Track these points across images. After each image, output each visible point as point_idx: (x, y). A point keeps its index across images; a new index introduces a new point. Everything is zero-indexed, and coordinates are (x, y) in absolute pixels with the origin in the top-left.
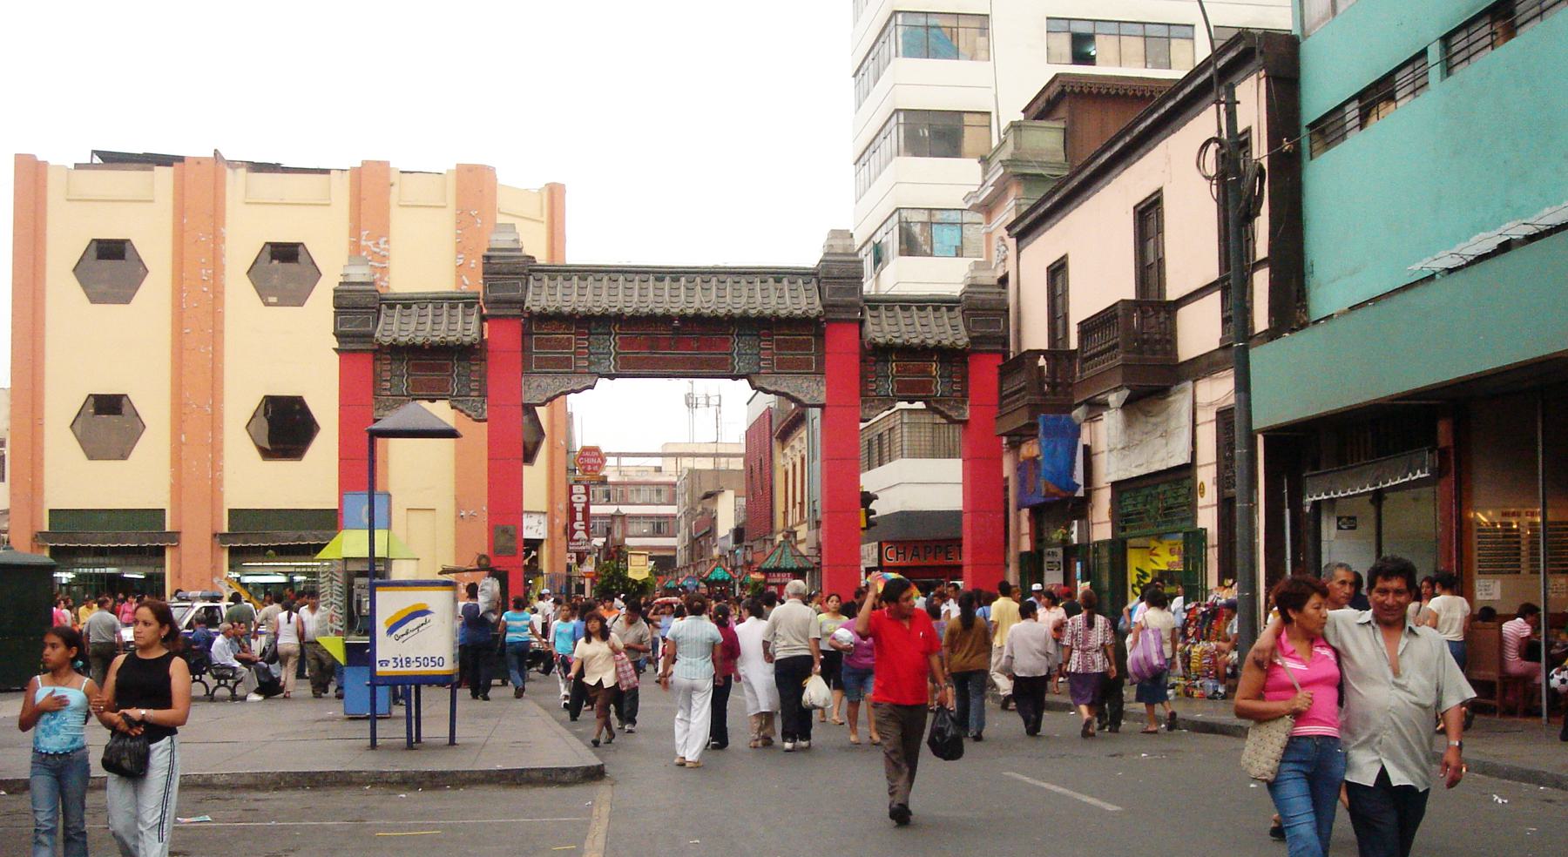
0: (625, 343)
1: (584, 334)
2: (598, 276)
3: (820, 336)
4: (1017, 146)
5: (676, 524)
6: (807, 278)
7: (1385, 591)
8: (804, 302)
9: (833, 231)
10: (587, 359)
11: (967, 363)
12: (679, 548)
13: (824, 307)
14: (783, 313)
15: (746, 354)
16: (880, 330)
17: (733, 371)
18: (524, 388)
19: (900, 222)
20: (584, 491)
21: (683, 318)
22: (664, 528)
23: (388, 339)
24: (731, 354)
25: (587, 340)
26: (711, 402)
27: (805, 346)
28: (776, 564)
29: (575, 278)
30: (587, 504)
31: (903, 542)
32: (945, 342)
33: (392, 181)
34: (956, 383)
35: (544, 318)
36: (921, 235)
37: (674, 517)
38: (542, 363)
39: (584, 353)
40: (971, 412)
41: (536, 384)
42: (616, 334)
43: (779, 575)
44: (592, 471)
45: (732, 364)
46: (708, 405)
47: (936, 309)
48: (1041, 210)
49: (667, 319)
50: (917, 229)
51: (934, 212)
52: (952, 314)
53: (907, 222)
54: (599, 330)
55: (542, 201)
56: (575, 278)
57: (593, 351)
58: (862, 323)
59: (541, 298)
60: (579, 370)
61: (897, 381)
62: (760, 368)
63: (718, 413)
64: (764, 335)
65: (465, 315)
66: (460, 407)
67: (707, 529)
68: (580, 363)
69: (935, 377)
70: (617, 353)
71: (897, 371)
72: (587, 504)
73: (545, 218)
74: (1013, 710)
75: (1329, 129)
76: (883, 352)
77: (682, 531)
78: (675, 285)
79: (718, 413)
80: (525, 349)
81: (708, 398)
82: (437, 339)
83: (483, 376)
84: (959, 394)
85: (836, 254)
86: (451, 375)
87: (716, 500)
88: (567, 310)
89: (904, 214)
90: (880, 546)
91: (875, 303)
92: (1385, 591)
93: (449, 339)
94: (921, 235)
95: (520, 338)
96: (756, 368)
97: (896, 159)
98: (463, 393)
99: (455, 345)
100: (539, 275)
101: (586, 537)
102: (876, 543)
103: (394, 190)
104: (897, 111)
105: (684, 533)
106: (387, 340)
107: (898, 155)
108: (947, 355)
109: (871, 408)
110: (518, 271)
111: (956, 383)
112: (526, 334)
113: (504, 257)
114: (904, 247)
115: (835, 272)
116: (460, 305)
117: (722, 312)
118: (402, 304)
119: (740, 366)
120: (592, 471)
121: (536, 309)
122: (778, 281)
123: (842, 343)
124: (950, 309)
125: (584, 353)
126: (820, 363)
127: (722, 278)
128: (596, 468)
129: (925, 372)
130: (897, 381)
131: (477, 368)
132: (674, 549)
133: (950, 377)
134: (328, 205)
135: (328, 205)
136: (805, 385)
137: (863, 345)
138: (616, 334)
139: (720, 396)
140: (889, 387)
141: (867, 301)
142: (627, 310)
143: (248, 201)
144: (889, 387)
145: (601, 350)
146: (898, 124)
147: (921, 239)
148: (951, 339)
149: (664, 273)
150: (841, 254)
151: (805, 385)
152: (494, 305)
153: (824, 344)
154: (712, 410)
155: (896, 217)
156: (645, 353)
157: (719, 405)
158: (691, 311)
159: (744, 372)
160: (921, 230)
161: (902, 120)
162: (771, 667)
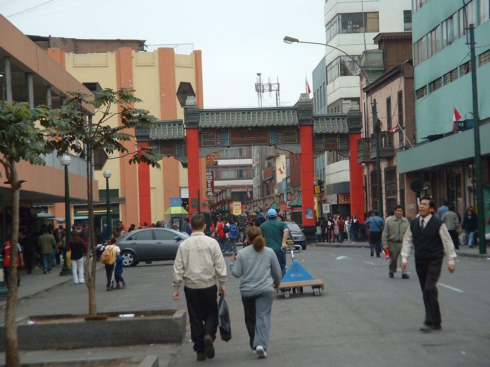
0: (233, 136)
1: (219, 133)
2: (223, 113)
3: (298, 130)
4: (366, 60)
5: (252, 171)
6: (293, 110)
7: (398, 211)
8: (292, 120)
9: (302, 94)
10: (220, 142)
11: (349, 137)
12: (254, 187)
13: (299, 121)
14: (285, 124)
15: (273, 138)
16: (320, 128)
17: (269, 144)
18: (200, 152)
19: (340, 62)
20: (211, 174)
21: (252, 127)
22: (245, 174)
23: (154, 138)
24: (269, 138)
25: (220, 135)
26: (273, 88)
27: (293, 134)
28: (296, 204)
29: (215, 114)
30: (213, 180)
31: (345, 194)
32: (341, 132)
33: (132, 56)
34: (345, 144)
35: (205, 129)
36: (350, 67)
37: (251, 166)
38: (205, 143)
39: (219, 140)
40: (351, 154)
41: (203, 150)
42: (230, 133)
43: (298, 208)
44: (210, 159)
45: (269, 141)
46: (270, 90)
47: (338, 119)
48: (380, 81)
49: (246, 128)
50: (347, 64)
51: (354, 56)
52: (344, 121)
53: (343, 61)
54: (224, 132)
55: (192, 61)
56: (215, 114)
57: (222, 139)
58: (312, 126)
59: (205, 122)
60: (218, 145)
61: (325, 145)
62: (279, 142)
63: (278, 95)
64: (279, 131)
65: (179, 128)
66: (178, 159)
67: (271, 177)
68: (218, 143)
69: (338, 143)
70: (230, 139)
71: (325, 141)
72: (213, 180)
73: (194, 66)
74: (85, 161)
75: (421, 92)
76: (320, 136)
77: (256, 176)
78: (249, 115)
79: (278, 95)
80: (199, 139)
81: (270, 85)
82: (170, 137)
83: (185, 148)
84: (347, 148)
85: (303, 102)
86: (175, 148)
87: (275, 160)
88: (213, 126)
89: (342, 58)
90: (338, 194)
91: (317, 118)
92: (398, 211)
93: (175, 137)
94: (350, 67)
95: (197, 135)
96: (277, 142)
97: (339, 35)
98: (179, 154)
99: (177, 139)
100: (203, 113)
101: (213, 194)
102: (336, 194)
103: (134, 59)
104: (338, 14)
105: (257, 177)
106: (154, 138)
107: (339, 33)
108: (342, 136)
109: (317, 154)
110: (196, 113)
111: (345, 144)
112: (200, 133)
113: (192, 108)
114: (343, 72)
115: (303, 109)
116: (177, 124)
117: (265, 125)
118: (178, 124)
119: (271, 142)
120: (210, 159)
121: (203, 126)
122: (284, 112)
123: (306, 132)
124: (343, 119)
125: (280, 137)
126: (299, 140)
127: (265, 112)
128: (212, 157)
129: (335, 141)
130: (325, 145)
131: (183, 146)
132: (251, 187)
133: (343, 142)
134: (107, 67)
135: (107, 67)
136: (294, 147)
137: (312, 134)
138: (230, 133)
139: (278, 84)
140: (322, 147)
141: (314, 117)
142: (233, 125)
143: (74, 66)
144: (322, 147)
145: (224, 138)
146: (339, 19)
147: (349, 68)
148: (343, 130)
149: (245, 111)
150: (305, 102)
151: (294, 147)
152: (189, 125)
153: (300, 133)
154: (274, 93)
155: (339, 58)
156: (240, 139)
157: (278, 90)
158: (254, 125)
159: (273, 144)
160: (349, 64)
161: (340, 18)
162: (121, 119)
